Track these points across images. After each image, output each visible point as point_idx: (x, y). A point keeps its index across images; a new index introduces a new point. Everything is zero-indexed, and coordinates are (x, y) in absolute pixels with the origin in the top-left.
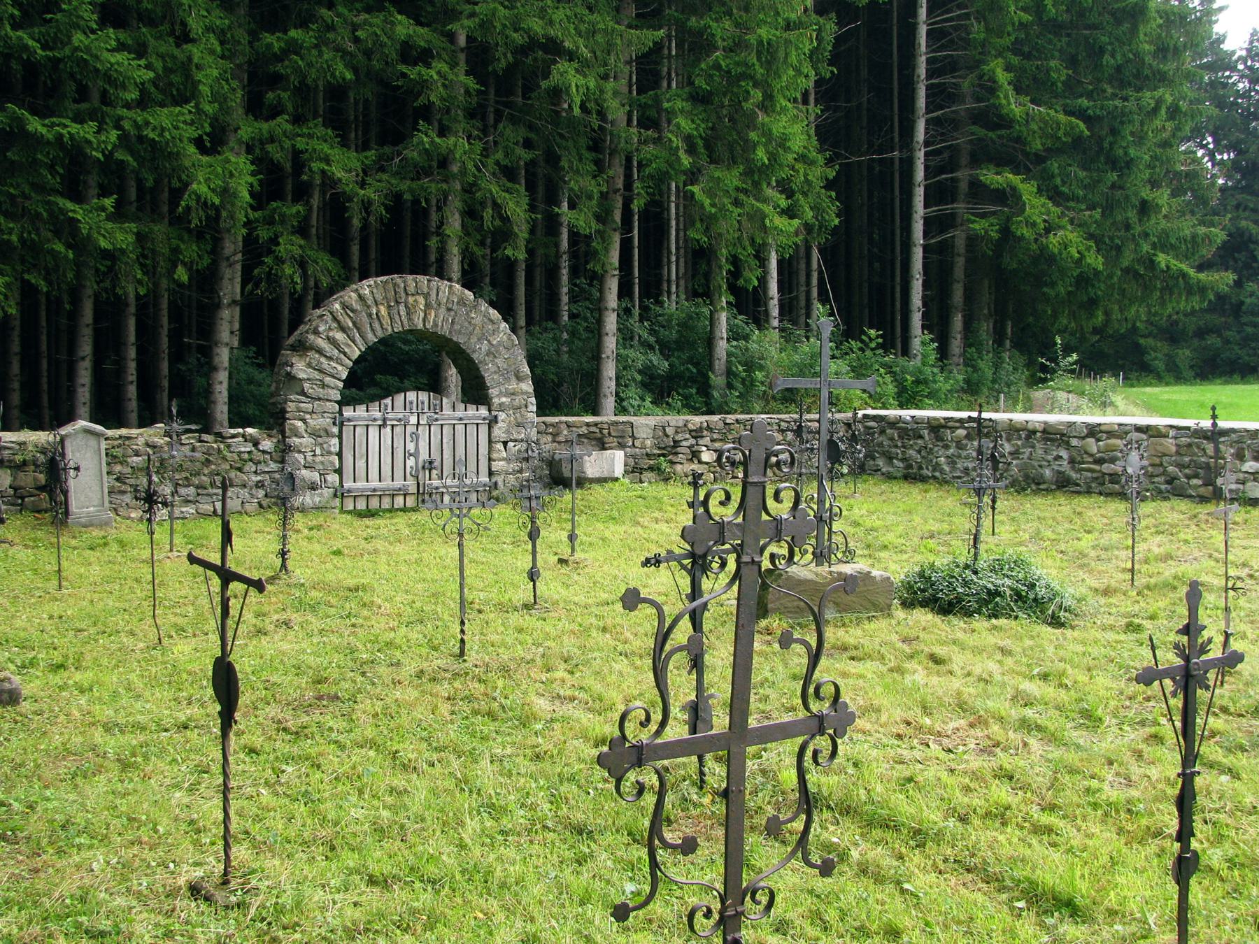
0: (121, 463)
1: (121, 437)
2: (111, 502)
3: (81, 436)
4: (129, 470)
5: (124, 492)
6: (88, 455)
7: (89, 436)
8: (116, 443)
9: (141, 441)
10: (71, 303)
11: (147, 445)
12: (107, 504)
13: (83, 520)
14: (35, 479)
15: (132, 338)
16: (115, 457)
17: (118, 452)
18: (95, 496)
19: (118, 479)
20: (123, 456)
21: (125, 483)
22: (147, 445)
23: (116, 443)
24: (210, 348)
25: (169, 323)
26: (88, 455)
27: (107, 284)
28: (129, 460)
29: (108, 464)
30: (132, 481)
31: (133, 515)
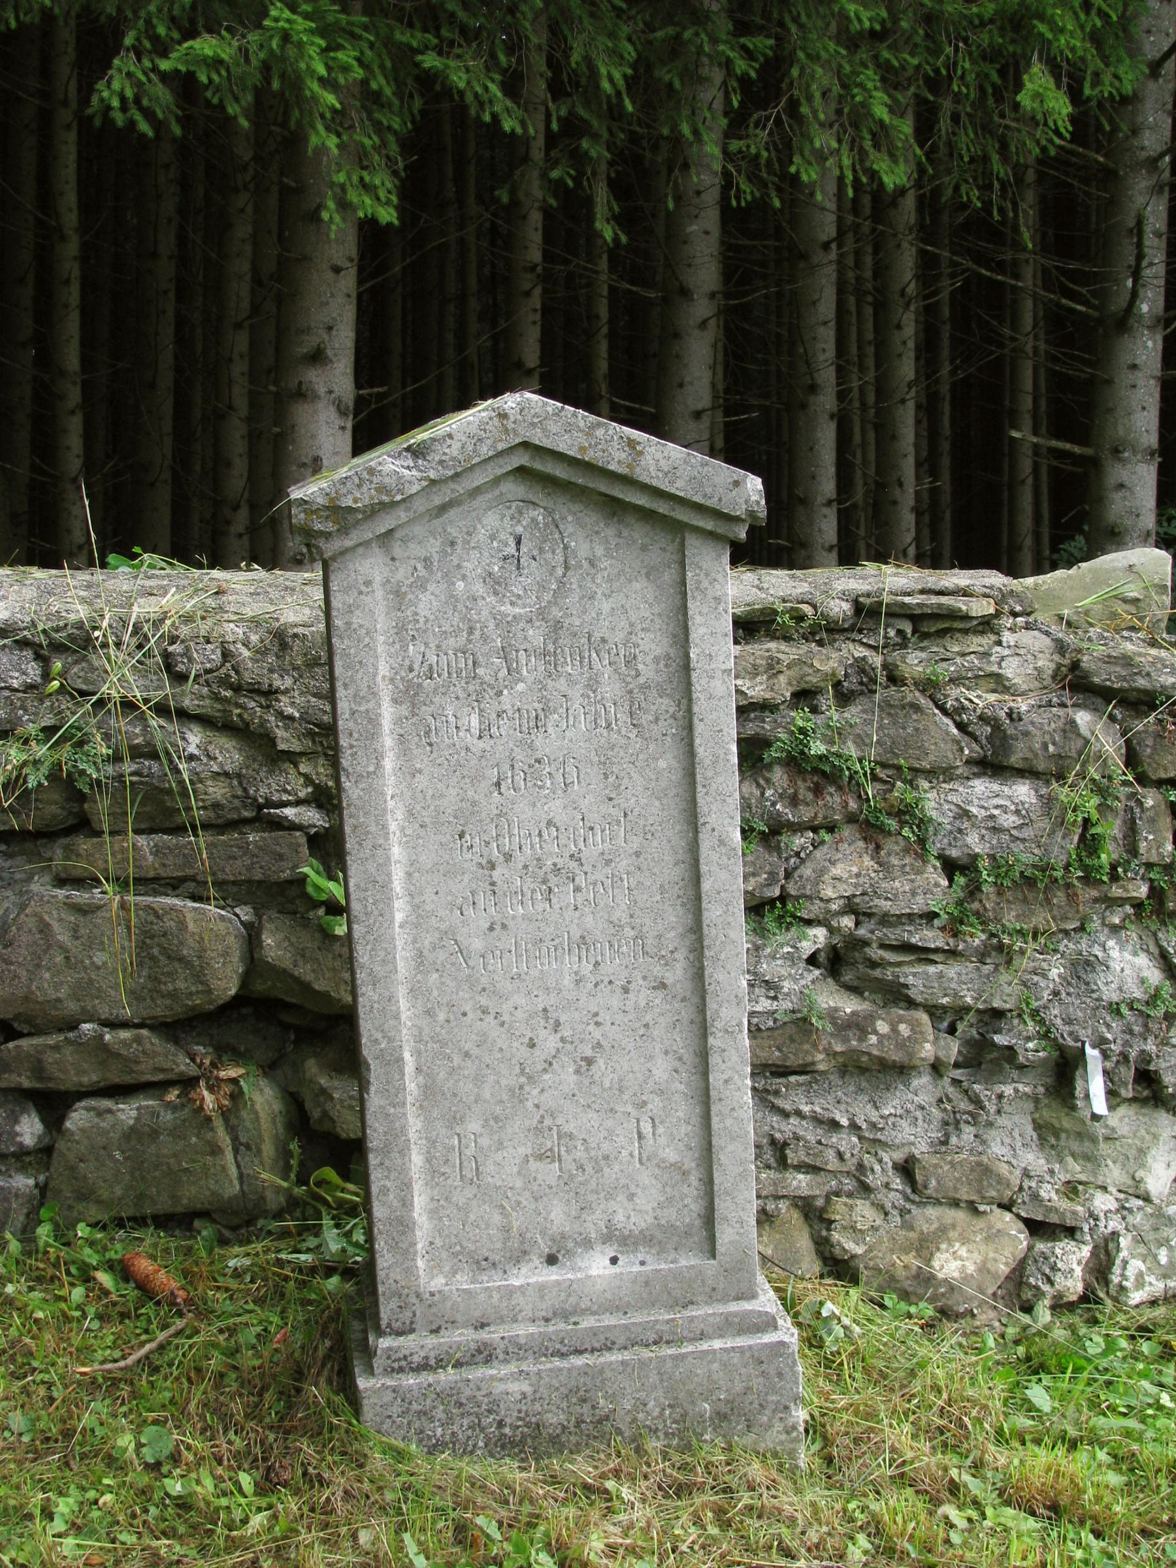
0: (871, 831)
1: (867, 612)
2: (777, 1152)
3: (493, 526)
4: (931, 888)
5: (889, 1071)
6: (569, 735)
7: (585, 537)
8: (832, 660)
9: (1023, 656)
10: (621, 220)
11: (1075, 682)
12: (742, 1186)
13: (507, 1383)
14: (156, 948)
15: (827, 486)
16: (822, 775)
17: (846, 734)
18: (635, 1147)
19: (834, 962)
20: (890, 769)
21: (896, 995)
22: (1075, 682)
23: (832, 660)
24: (1095, 464)
25: (918, 477)
26: (569, 735)
27: (758, 142)
28: (934, 802)
29: (765, 833)
30: (956, 981)
31: (952, 1263)
